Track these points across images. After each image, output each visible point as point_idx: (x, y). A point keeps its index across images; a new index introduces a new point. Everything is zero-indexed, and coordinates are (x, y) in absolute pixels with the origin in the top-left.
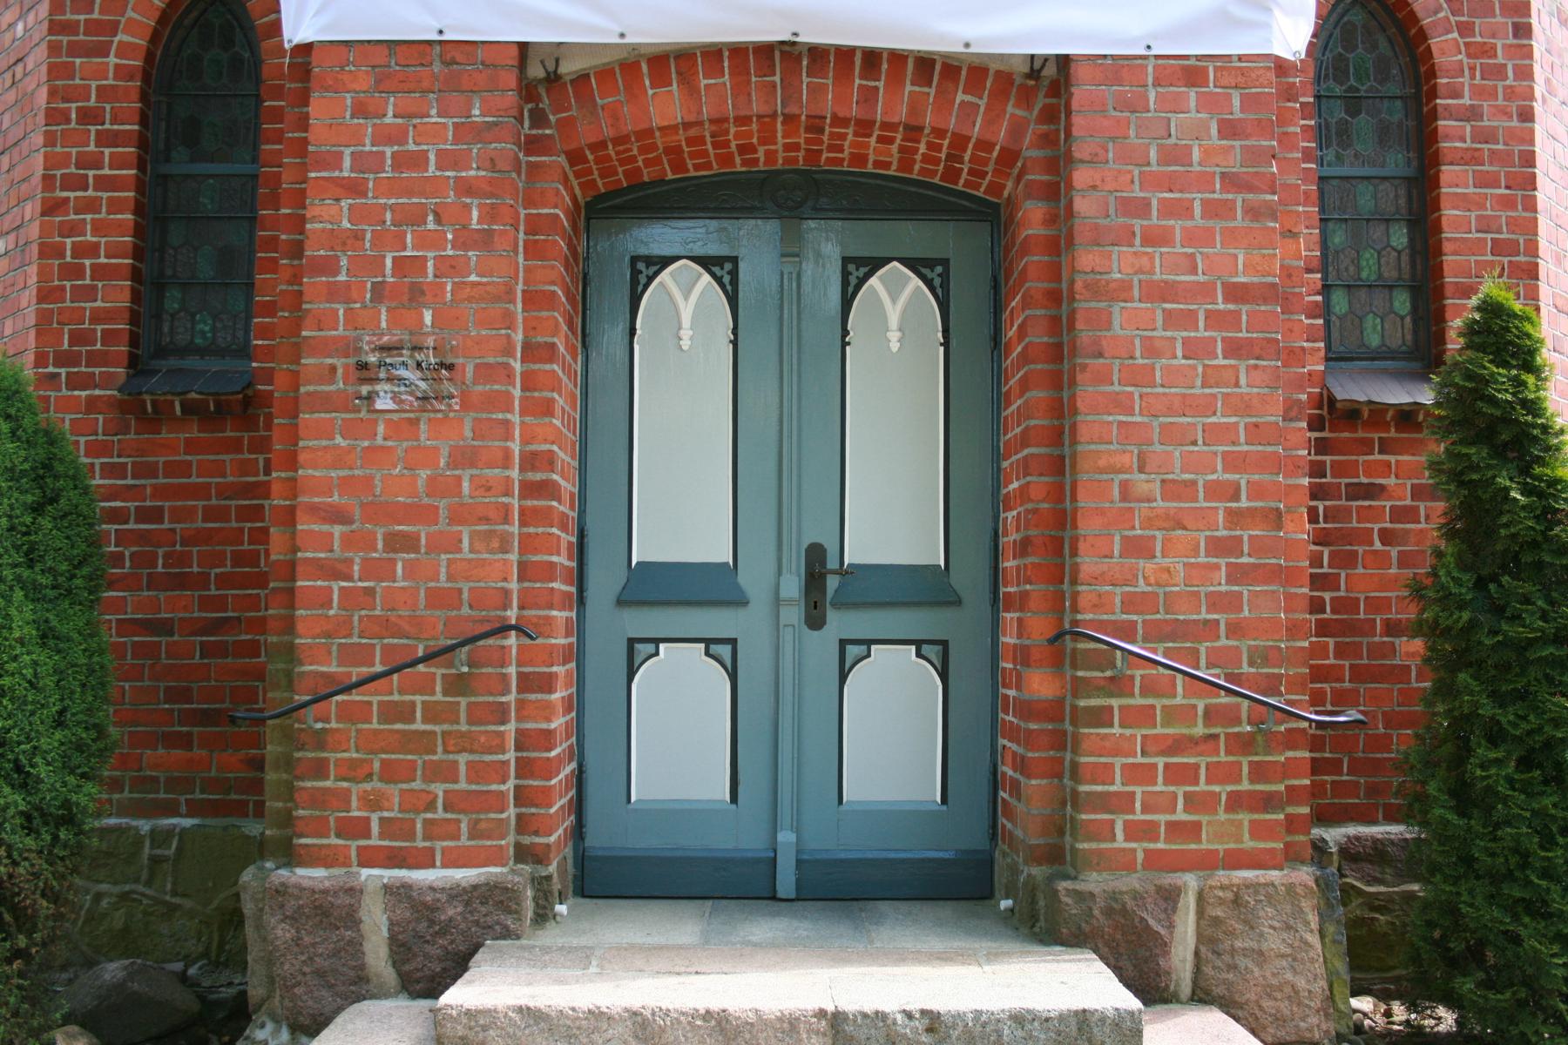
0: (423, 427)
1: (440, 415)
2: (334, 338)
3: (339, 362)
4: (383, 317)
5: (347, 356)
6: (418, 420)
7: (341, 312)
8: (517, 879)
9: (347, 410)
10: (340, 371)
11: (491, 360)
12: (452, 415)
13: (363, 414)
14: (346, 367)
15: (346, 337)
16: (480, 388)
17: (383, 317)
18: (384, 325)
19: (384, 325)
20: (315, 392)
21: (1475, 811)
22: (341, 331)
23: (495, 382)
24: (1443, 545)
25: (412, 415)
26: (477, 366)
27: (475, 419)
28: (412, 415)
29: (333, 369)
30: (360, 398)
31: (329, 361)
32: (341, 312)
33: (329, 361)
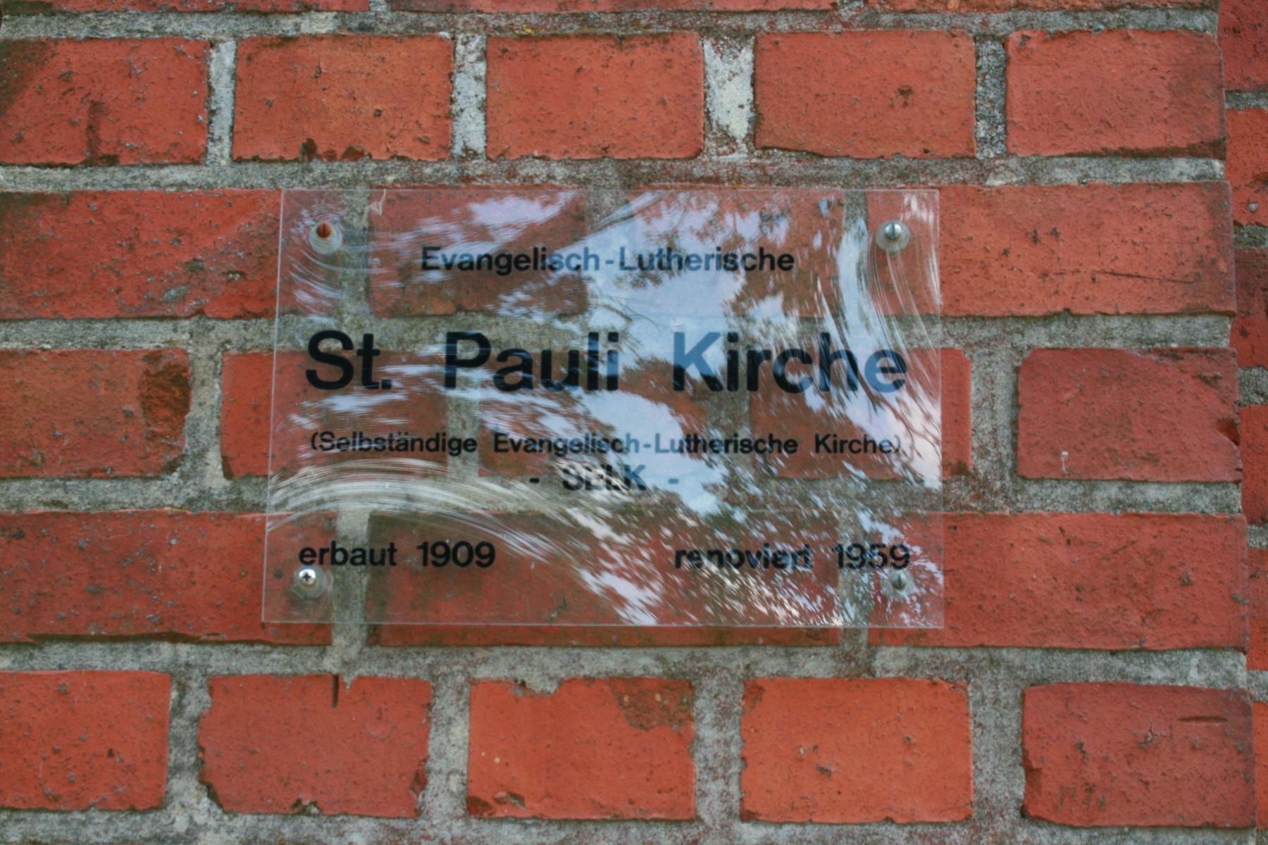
0: (712, 735)
1: (816, 665)
2: (177, 199)
3: (205, 345)
4: (469, 88)
5: (253, 303)
6: (681, 687)
7: (223, 60)
8: (300, 536)
9: (254, 636)
10: (208, 398)
11: (1119, 334)
12: (890, 660)
13: (344, 654)
14: (246, 367)
15: (249, 201)
16: (1053, 499)
17: (469, 88)
18: (471, 129)
19: (471, 129)
20: (57, 520)
21: (819, 599)
22: (218, 167)
23: (1156, 463)
24: (164, 362)
25: (642, 663)
26: (1029, 368)
27: (1033, 691)
28: (642, 663)
29: (169, 385)
30: (326, 552)
31: (149, 336)
32: (223, 60)
33: (149, 336)
